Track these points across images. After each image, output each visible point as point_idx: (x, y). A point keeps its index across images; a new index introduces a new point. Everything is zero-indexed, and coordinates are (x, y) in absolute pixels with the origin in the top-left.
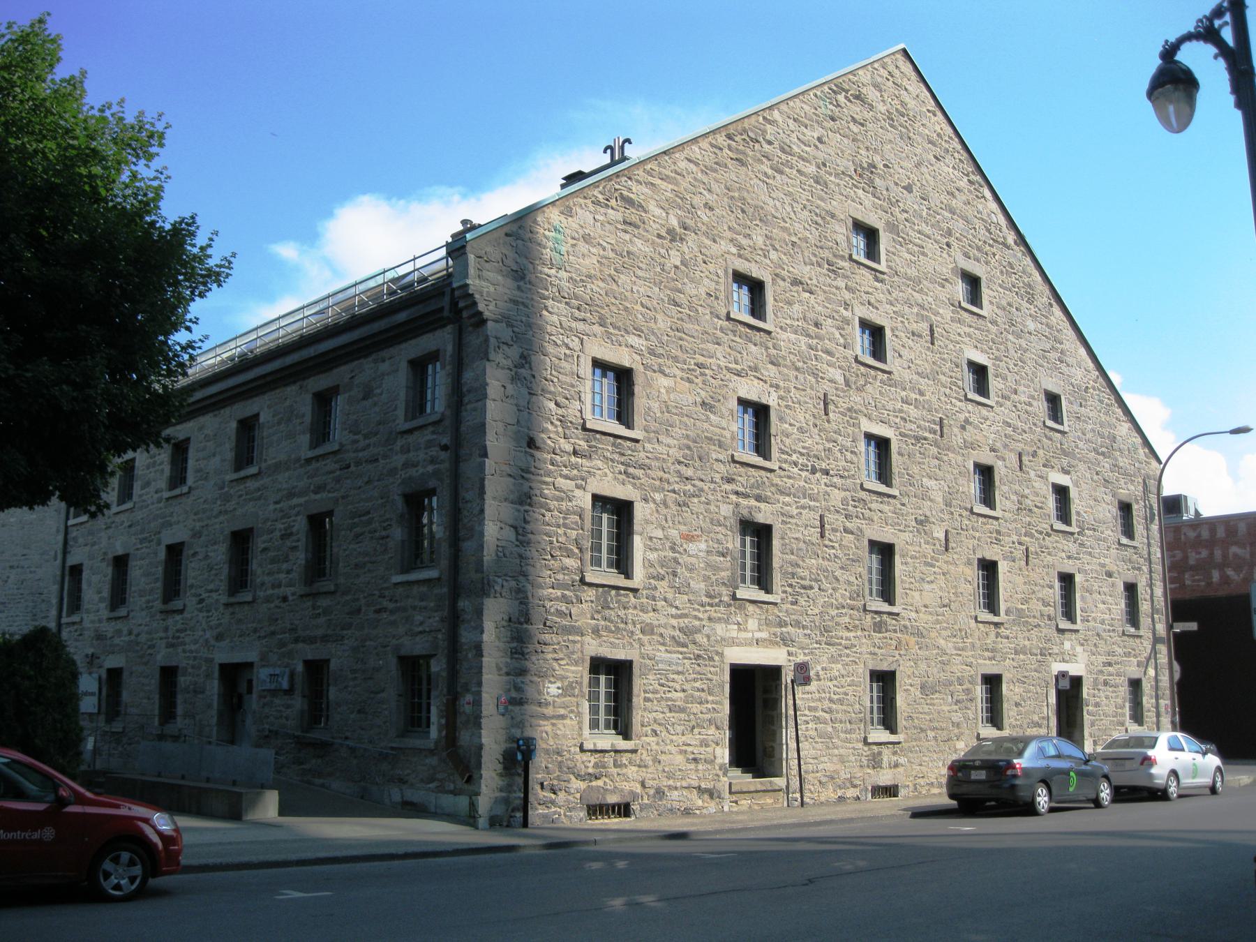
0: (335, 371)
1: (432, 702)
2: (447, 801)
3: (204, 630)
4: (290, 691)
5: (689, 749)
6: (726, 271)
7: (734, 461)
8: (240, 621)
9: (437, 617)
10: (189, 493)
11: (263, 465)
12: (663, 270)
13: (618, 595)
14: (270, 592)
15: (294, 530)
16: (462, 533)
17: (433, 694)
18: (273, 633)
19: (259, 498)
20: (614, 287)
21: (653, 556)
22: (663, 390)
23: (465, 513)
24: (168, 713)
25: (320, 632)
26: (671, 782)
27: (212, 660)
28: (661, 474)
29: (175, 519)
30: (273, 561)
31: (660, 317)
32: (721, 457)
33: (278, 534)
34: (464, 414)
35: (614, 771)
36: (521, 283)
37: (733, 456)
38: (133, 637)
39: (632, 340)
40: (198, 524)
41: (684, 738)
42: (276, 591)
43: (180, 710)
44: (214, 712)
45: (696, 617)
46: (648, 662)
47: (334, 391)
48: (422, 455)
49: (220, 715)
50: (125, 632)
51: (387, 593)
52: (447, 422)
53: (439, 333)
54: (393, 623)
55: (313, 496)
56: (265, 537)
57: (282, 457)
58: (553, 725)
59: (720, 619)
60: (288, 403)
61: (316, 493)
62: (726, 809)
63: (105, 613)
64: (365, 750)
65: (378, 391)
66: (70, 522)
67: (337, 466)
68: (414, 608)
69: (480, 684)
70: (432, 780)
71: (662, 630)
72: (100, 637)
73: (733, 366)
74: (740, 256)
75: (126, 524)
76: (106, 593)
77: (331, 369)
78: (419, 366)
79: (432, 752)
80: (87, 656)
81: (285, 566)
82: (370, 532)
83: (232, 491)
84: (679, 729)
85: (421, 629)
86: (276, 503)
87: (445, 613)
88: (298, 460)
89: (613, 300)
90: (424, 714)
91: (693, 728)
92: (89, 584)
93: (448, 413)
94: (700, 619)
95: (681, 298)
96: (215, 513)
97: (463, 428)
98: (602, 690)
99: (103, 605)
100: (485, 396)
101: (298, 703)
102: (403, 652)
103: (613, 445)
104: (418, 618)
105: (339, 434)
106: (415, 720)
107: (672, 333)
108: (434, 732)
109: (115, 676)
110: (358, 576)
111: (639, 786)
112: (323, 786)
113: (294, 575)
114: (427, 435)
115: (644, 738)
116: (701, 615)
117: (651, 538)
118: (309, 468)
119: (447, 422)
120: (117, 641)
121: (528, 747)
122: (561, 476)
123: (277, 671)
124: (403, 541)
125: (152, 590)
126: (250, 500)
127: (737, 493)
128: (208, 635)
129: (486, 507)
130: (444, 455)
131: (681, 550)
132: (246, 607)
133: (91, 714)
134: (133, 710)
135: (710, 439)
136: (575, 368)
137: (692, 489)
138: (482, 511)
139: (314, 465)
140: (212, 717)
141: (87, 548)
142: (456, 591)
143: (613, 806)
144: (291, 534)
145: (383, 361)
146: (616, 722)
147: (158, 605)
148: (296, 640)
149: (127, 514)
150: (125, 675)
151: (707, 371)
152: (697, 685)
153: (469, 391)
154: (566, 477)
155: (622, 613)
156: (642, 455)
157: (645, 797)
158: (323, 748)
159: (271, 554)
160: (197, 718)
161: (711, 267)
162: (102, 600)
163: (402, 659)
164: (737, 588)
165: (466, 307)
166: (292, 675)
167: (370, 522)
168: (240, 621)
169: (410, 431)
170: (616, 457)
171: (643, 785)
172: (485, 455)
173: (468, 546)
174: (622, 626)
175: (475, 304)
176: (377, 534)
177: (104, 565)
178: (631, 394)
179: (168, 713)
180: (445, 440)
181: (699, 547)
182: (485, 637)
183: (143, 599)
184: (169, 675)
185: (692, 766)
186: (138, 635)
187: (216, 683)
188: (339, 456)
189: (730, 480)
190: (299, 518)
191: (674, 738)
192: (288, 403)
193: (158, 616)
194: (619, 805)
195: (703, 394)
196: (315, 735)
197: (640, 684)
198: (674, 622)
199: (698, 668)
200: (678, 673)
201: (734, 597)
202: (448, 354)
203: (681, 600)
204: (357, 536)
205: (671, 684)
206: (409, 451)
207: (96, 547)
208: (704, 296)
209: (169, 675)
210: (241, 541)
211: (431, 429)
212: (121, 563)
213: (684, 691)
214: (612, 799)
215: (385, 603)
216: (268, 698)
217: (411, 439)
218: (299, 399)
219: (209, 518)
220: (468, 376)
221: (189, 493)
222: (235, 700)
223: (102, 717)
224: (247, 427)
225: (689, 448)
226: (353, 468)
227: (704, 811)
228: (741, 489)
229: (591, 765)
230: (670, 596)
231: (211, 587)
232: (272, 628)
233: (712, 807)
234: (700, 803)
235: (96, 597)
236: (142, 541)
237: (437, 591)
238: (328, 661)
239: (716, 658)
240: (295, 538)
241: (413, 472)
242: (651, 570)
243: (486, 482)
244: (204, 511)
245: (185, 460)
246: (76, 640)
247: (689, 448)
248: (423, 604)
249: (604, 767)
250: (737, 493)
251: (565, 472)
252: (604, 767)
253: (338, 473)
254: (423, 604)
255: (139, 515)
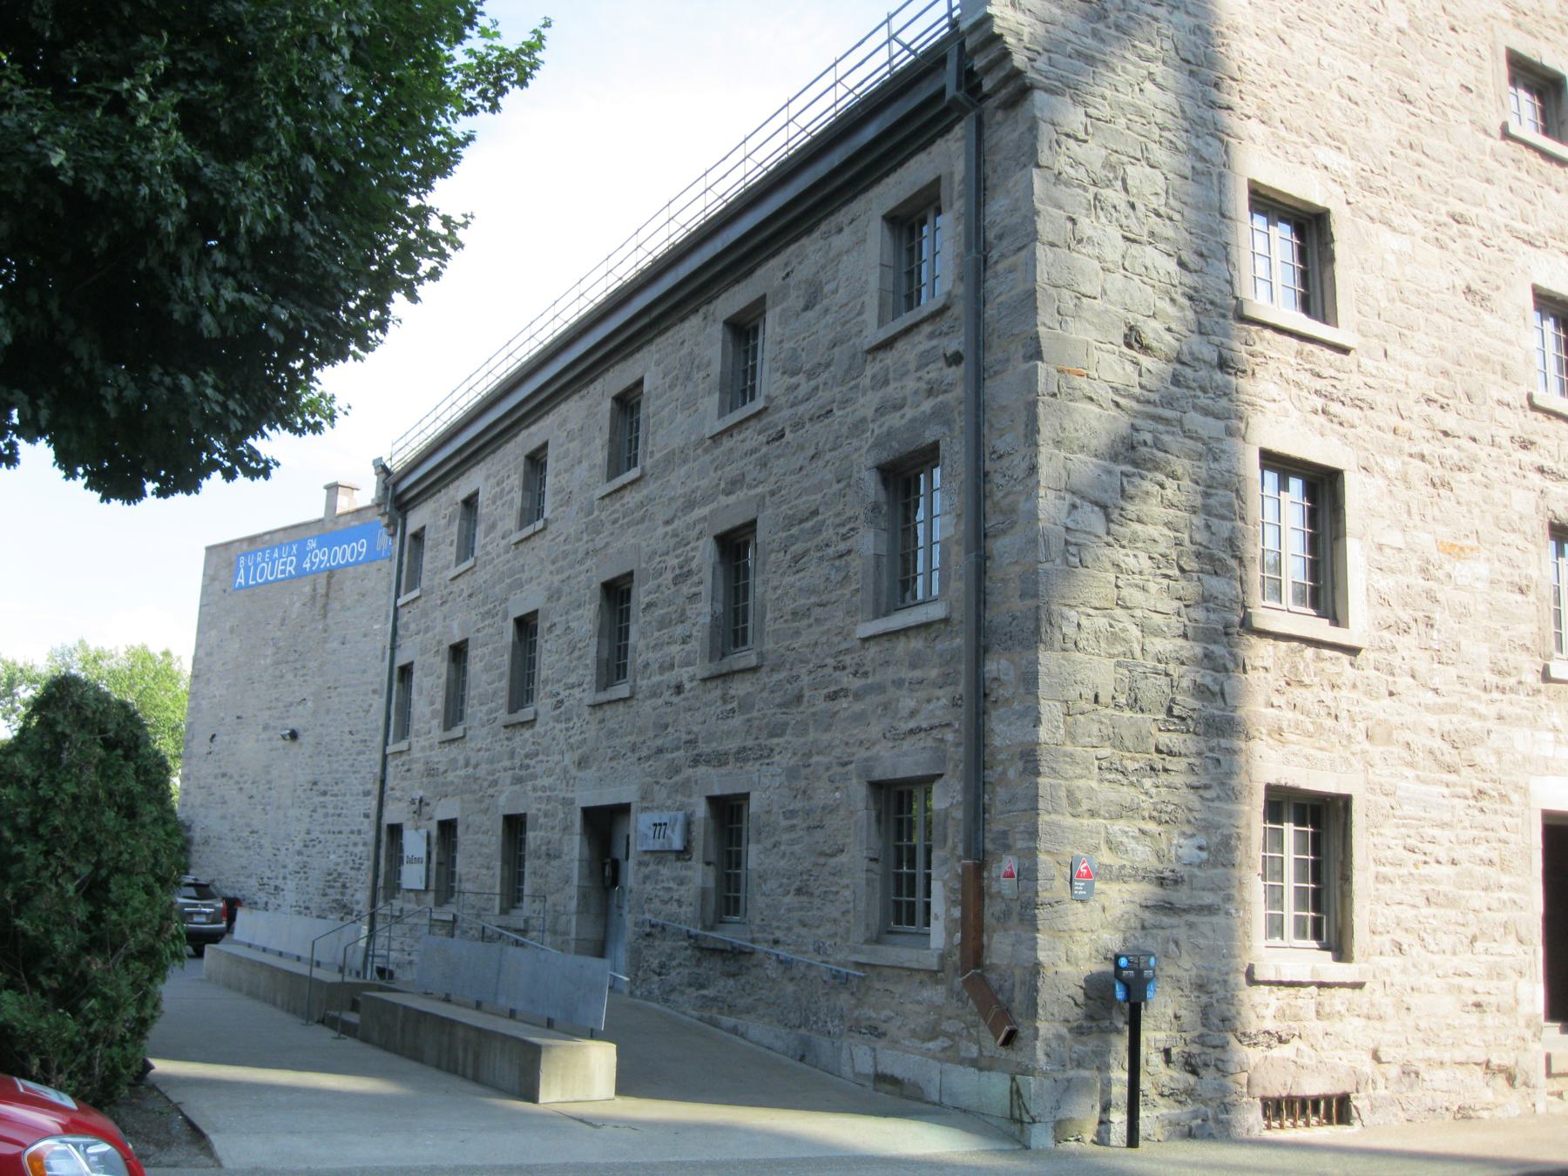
0: (760, 272)
1: (934, 873)
2: (965, 1082)
3: (562, 753)
4: (684, 854)
5: (1467, 983)
6: (1493, 49)
7: (1534, 408)
8: (611, 733)
9: (944, 696)
10: (544, 528)
11: (649, 462)
12: (1375, 32)
13: (1319, 658)
14: (656, 679)
15: (694, 565)
16: (992, 521)
17: (936, 855)
18: (660, 751)
19: (642, 520)
20: (1284, 51)
21: (1385, 583)
22: (1390, 258)
23: (997, 479)
24: (513, 894)
25: (732, 745)
26: (1432, 1052)
27: (572, 801)
28: (1394, 420)
29: (525, 576)
30: (663, 624)
31: (1376, 117)
32: (1507, 397)
33: (669, 575)
34: (991, 283)
35: (1317, 1026)
36: (1100, 26)
37: (1530, 397)
38: (470, 770)
39: (1325, 155)
40: (557, 578)
41: (1456, 961)
42: (666, 676)
43: (527, 889)
44: (573, 890)
45: (1473, 712)
46: (1382, 800)
47: (758, 308)
48: (911, 384)
49: (583, 896)
50: (461, 762)
51: (848, 659)
52: (958, 309)
53: (940, 147)
54: (861, 718)
55: (724, 500)
56: (651, 584)
57: (677, 442)
58: (1191, 926)
59: (1519, 718)
60: (686, 350)
61: (728, 493)
62: (1541, 1108)
63: (438, 734)
64: (809, 966)
65: (832, 286)
66: (400, 602)
67: (763, 438)
68: (899, 683)
69: (1033, 834)
70: (933, 1033)
71: (1408, 736)
72: (431, 772)
73: (1519, 225)
74: (1518, 26)
75: (466, 594)
76: (439, 704)
77: (751, 271)
78: (907, 223)
79: (933, 974)
80: (413, 802)
81: (679, 630)
82: (819, 548)
83: (603, 517)
84: (1447, 941)
85: (912, 725)
86: (667, 523)
87: (961, 689)
88: (701, 442)
89: (1284, 77)
90: (919, 897)
91: (1474, 939)
92: (421, 694)
93: (960, 290)
94: (1481, 717)
95: (1411, 88)
96: (580, 555)
97: (990, 311)
98: (1290, 855)
99: (435, 722)
100: (1033, 236)
101: (699, 875)
102: (879, 774)
103: (1299, 353)
104: (908, 703)
105: (770, 381)
106: (904, 910)
107: (1399, 151)
108: (938, 935)
109: (448, 828)
110: (797, 633)
111: (1368, 1058)
112: (734, 1030)
113: (694, 645)
114: (921, 342)
115: (1377, 959)
116: (1482, 709)
117: (1380, 547)
118: (717, 452)
119: (958, 309)
120: (451, 776)
121: (1139, 972)
122: (1195, 407)
123: (665, 817)
124: (877, 556)
125: (495, 693)
126: (629, 525)
127: (1541, 470)
128: (569, 759)
129: (1042, 460)
130: (955, 373)
131: (1440, 574)
132: (621, 707)
133: (417, 891)
134: (467, 886)
135: (1487, 361)
136: (1215, 197)
137: (1456, 455)
138: (1033, 469)
139: (727, 443)
140: (568, 898)
141: (419, 638)
142: (981, 644)
143: (1316, 1102)
144: (690, 573)
145: (840, 230)
146: (1317, 923)
147: (503, 716)
148: (696, 762)
149: (467, 577)
150: (460, 830)
151: (1471, 230)
152: (1481, 850)
153: (1000, 237)
154: (1206, 412)
155: (1328, 696)
156: (1357, 379)
157: (1381, 1083)
158: (734, 956)
159: (659, 612)
160: (550, 899)
161: (1464, 38)
162: (434, 714)
163: (879, 788)
164: (1550, 657)
165: (988, 69)
166: (688, 825)
167: (817, 530)
168: (611, 733)
169: (887, 344)
170: (1305, 378)
171: (1376, 1057)
172: (1037, 354)
173: (1003, 547)
174: (1330, 722)
175: (1006, 55)
176: (831, 551)
177: (439, 659)
178: (1328, 258)
179: (513, 894)
180: (954, 344)
181: (1474, 570)
182: (1043, 733)
183: (484, 708)
184: (515, 826)
185: (1474, 1018)
186: (476, 767)
187: (577, 839)
188: (765, 420)
189: (1526, 445)
190: (701, 543)
191: (1437, 959)
192: (686, 350)
193: (503, 734)
194: (1328, 1099)
195: (1467, 272)
196: (729, 934)
197: (1368, 844)
198: (1431, 720)
199: (1480, 817)
200: (1444, 825)
201: (1546, 676)
202: (958, 177)
203: (1443, 677)
204: (796, 559)
205: (1428, 847)
206: (886, 382)
207: (430, 634)
208: (1457, 90)
209: (515, 826)
210: (616, 593)
211: (927, 329)
212: (458, 653)
213: (1454, 863)
214: (1312, 1087)
215: (847, 680)
216: (652, 867)
217: (889, 358)
218: (702, 337)
219: (571, 567)
220: (997, 207)
221: (544, 528)
222: (608, 870)
223: (430, 897)
224: (627, 403)
225: (1445, 373)
226: (789, 436)
227: (1498, 1113)
228: (1548, 464)
229: (1269, 1012)
230: (1422, 666)
231: (572, 679)
232: (659, 742)
233: (1511, 1103)
234: (1488, 1096)
235: (427, 711)
236: (485, 616)
237: (943, 645)
238: (746, 796)
239: (1515, 797)
240: (696, 579)
241: (894, 420)
242: (1385, 611)
243: (1041, 409)
244: (565, 555)
245: (542, 482)
246: (404, 779)
247: (1445, 373)
248: (917, 674)
249: (1296, 1018)
250: (1541, 470)
251: (1203, 401)
252: (1296, 1018)
253: (764, 449)
254: (917, 674)
255: (482, 576)
